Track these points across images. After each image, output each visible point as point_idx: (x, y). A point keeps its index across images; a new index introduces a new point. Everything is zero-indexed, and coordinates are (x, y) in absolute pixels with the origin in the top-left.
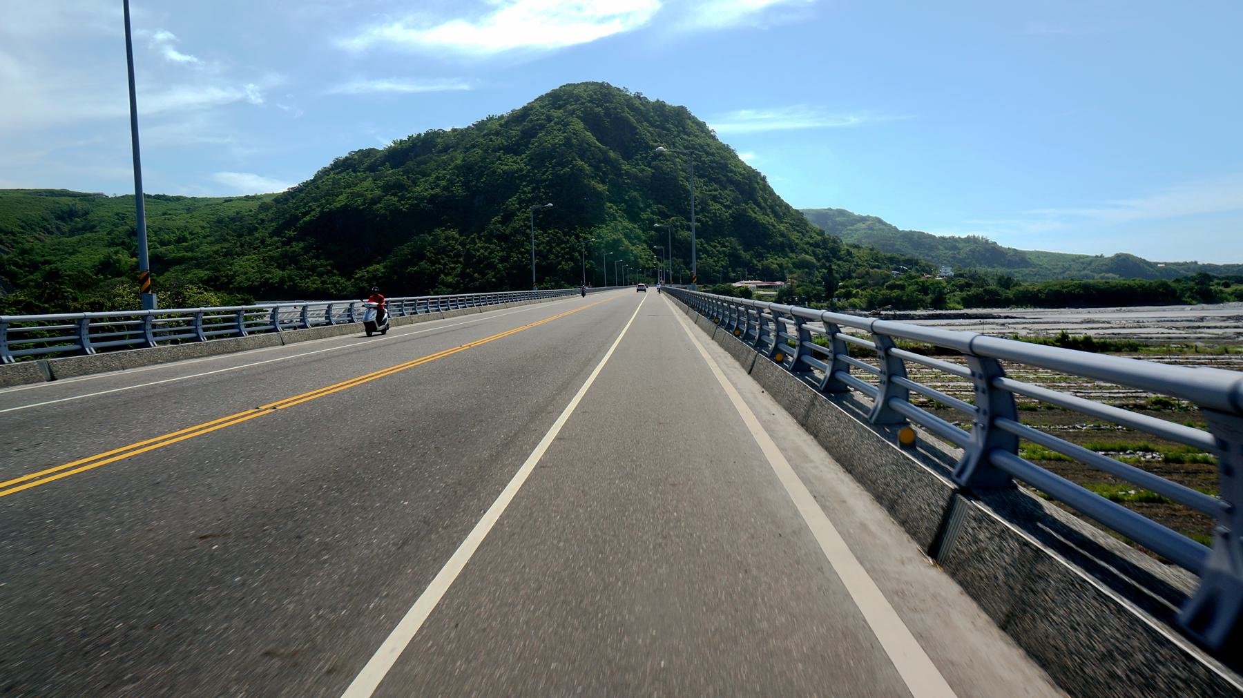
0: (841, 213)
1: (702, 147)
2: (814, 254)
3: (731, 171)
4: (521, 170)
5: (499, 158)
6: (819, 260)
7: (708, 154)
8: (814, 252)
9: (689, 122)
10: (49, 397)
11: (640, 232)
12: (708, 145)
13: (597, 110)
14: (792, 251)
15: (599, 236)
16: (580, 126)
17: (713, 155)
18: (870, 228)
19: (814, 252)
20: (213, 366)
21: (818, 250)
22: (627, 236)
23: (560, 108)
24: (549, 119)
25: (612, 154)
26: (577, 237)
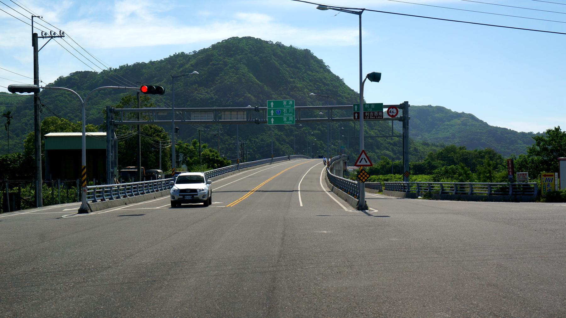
0: (440, 109)
1: (321, 80)
2: (393, 151)
3: (340, 96)
4: (212, 98)
5: (196, 89)
6: (395, 154)
7: (325, 84)
8: (392, 149)
9: (312, 61)
10: (244, 174)
11: (285, 137)
12: (325, 78)
13: (256, 58)
14: (378, 149)
15: (262, 140)
16: (245, 69)
17: (328, 85)
18: (464, 124)
19: (392, 149)
20: (255, 171)
21: (395, 148)
22: (278, 140)
23: (231, 56)
24: (225, 64)
25: (266, 88)
26: (250, 140)
